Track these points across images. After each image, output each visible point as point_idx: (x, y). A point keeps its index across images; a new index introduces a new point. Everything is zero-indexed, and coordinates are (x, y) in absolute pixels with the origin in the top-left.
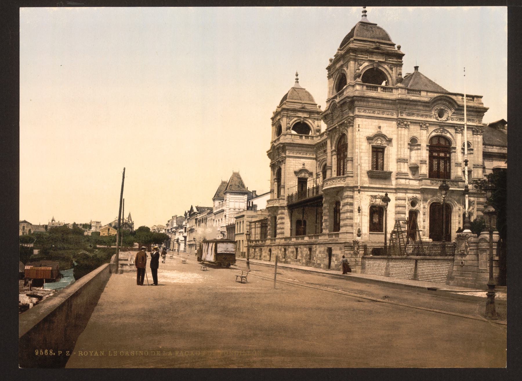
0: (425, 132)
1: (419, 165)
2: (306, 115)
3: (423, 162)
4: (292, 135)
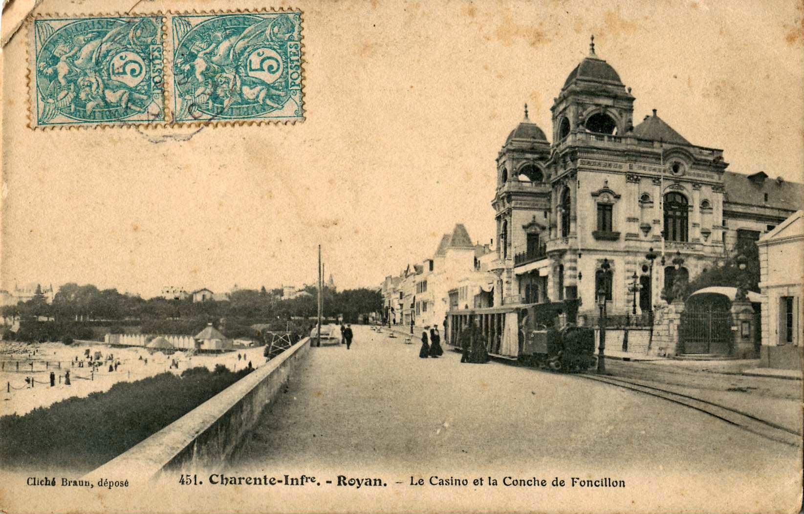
0: (657, 188)
1: (652, 225)
2: (609, 102)
3: (656, 222)
4: (587, 133)
